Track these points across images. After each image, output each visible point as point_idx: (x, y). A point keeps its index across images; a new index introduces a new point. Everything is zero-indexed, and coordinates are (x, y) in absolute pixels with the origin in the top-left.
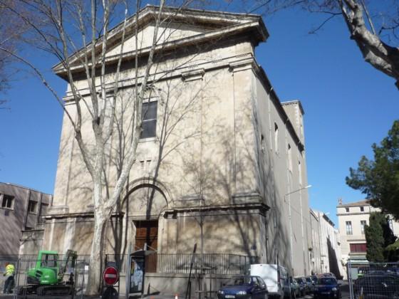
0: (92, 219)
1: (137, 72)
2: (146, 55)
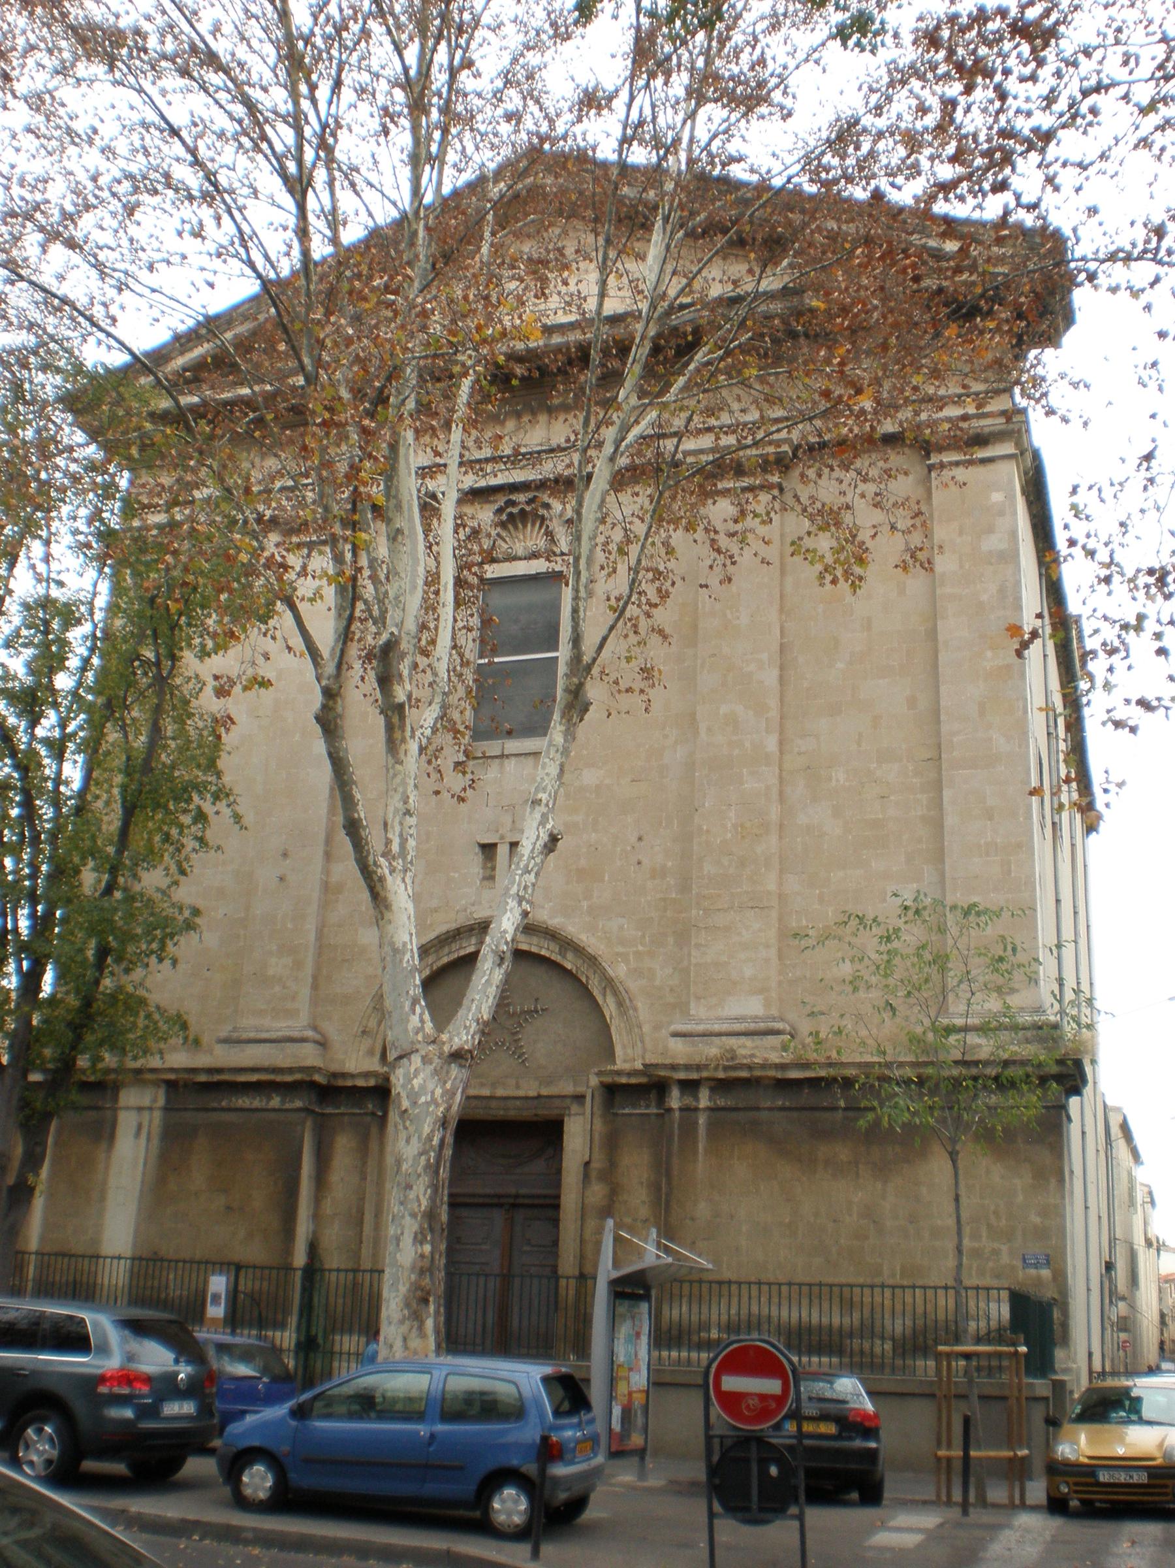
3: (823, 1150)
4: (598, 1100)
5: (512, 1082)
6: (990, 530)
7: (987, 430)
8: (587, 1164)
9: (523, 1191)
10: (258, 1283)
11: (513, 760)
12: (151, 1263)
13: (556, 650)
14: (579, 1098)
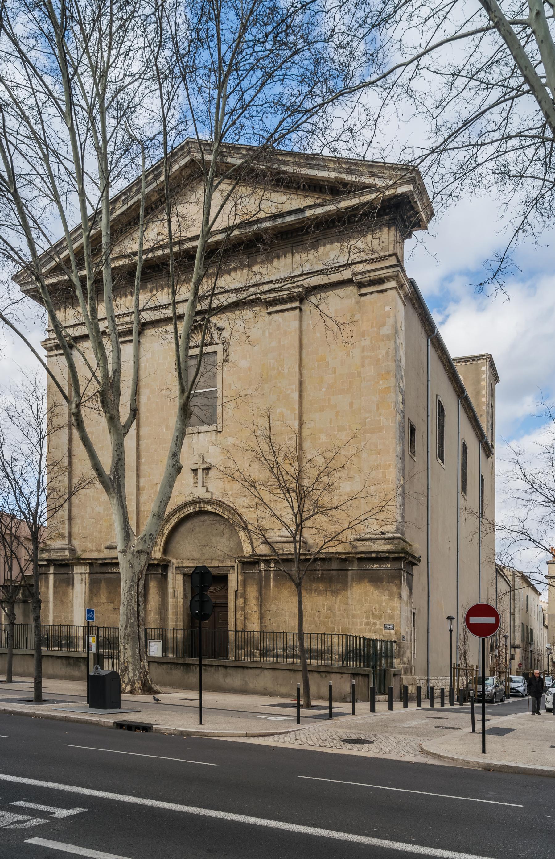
0: (115, 570)
1: (174, 293)
2: (190, 255)
3: (314, 586)
5: (209, 561)
6: (384, 325)
7: (383, 276)
9: (218, 601)
11: (202, 434)
14: (233, 567)
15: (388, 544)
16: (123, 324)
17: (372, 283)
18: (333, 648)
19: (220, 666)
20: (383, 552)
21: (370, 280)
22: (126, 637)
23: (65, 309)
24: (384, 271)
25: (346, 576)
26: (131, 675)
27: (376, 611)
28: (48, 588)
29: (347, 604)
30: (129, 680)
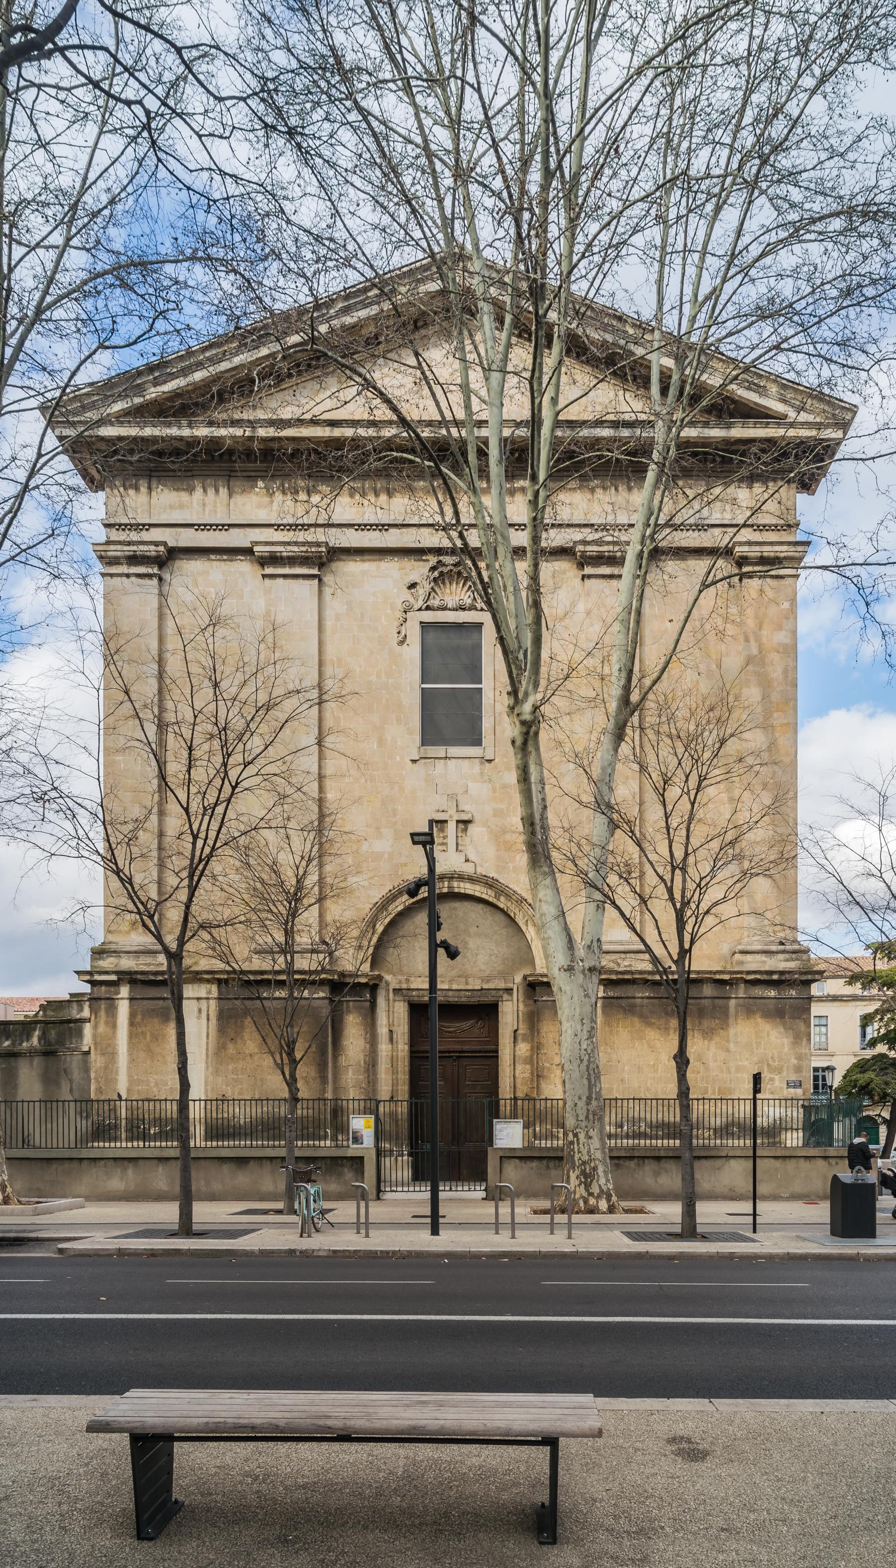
4: (521, 991)
7: (782, 555)
8: (515, 1031)
9: (466, 1048)
10: (305, 1111)
12: (316, 1102)
13: (481, 683)
14: (509, 991)
15: (792, 960)
16: (303, 544)
17: (763, 560)
18: (707, 1119)
19: (648, 1157)
20: (789, 972)
21: (762, 557)
22: (591, 1117)
23: (150, 488)
24: (785, 548)
25: (727, 1008)
26: (602, 1181)
27: (774, 1061)
28: (114, 1026)
29: (728, 1051)
30: (602, 1190)
